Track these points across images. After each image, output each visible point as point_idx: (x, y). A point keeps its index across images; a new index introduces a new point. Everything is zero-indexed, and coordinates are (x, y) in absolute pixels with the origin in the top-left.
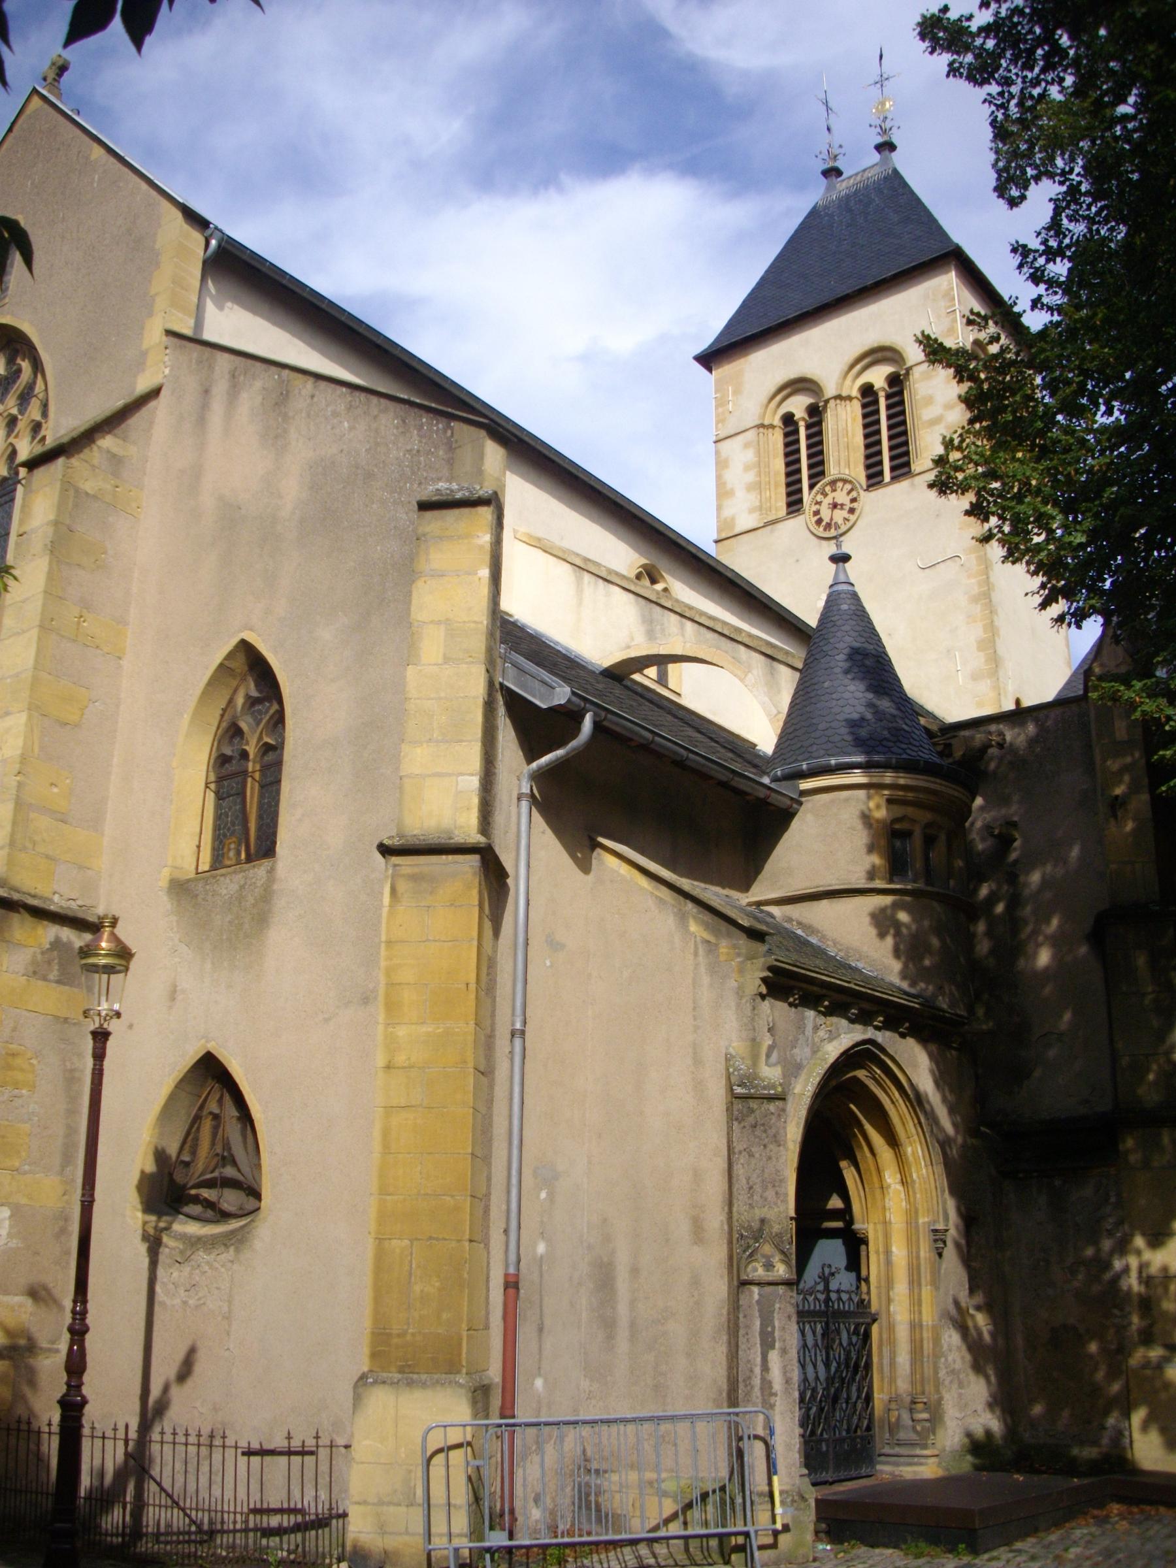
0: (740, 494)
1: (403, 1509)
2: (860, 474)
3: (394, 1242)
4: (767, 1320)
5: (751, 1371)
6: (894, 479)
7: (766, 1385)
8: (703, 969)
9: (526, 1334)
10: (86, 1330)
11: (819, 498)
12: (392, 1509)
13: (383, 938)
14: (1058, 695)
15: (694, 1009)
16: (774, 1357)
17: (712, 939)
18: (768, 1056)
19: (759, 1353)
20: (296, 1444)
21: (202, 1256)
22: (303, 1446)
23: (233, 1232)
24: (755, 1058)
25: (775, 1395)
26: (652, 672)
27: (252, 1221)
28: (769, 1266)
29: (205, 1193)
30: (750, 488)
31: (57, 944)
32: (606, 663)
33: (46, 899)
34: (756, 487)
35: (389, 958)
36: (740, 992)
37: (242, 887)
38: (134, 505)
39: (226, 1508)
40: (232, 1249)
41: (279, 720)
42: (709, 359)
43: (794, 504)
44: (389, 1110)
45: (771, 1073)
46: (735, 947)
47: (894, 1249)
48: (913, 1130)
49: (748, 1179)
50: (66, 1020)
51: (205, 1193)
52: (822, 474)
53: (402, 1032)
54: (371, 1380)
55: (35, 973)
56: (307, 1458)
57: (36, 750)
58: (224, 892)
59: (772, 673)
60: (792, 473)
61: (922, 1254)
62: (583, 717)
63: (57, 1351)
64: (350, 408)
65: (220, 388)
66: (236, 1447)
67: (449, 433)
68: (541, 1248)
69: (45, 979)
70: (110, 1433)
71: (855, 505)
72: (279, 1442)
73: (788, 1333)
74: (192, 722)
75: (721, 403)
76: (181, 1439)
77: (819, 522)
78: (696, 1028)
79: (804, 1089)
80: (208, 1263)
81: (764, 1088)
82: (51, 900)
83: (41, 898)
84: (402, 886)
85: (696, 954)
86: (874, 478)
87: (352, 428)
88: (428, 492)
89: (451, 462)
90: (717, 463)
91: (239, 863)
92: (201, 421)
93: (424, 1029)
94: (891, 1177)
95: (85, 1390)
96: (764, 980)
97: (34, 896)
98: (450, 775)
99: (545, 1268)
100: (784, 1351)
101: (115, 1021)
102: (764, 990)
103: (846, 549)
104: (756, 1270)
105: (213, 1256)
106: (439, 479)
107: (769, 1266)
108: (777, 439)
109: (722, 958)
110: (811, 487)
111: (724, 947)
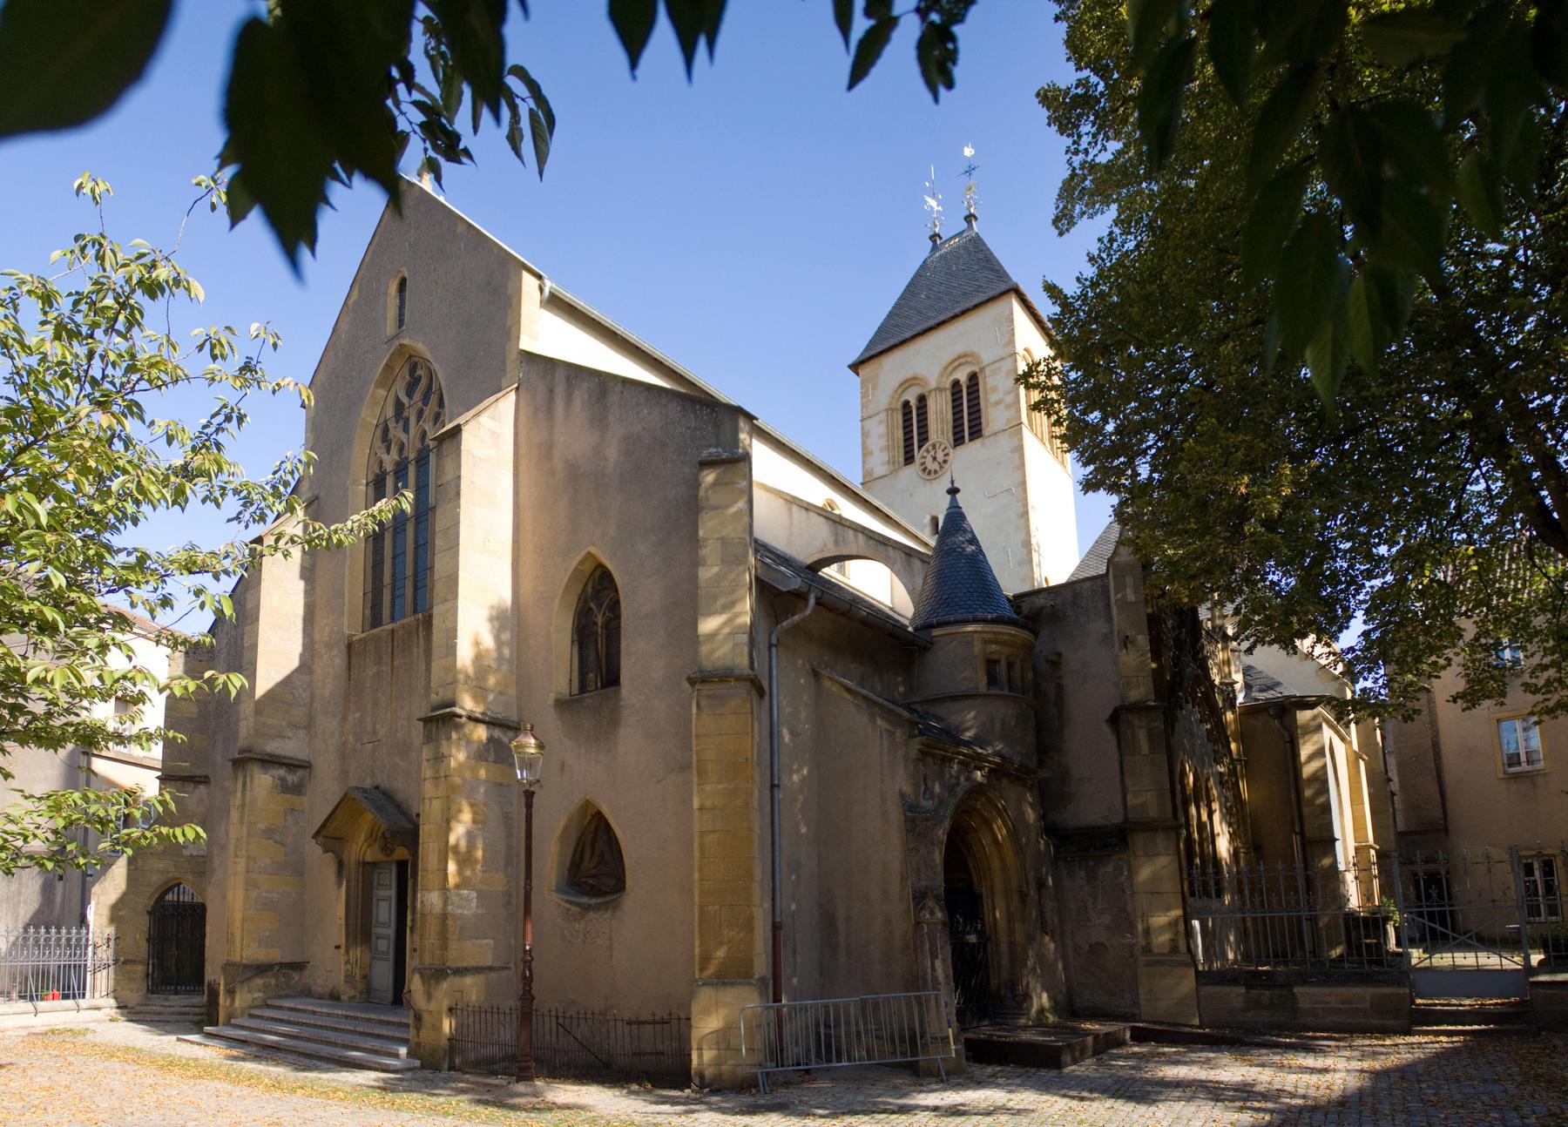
0: (877, 453)
6: (970, 440)
7: (935, 978)
14: (1073, 575)
16: (938, 963)
20: (658, 1018)
21: (591, 915)
26: (835, 566)
28: (932, 913)
30: (882, 450)
32: (809, 561)
34: (887, 448)
35: (698, 745)
41: (615, 605)
42: (855, 367)
50: (501, 784)
52: (926, 439)
53: (708, 788)
59: (909, 564)
65: (560, 390)
69: (486, 760)
72: (645, 1016)
75: (864, 395)
76: (589, 1015)
78: (882, 781)
84: (704, 703)
85: (881, 738)
86: (958, 441)
90: (863, 434)
91: (596, 689)
93: (720, 786)
100: (944, 960)
106: (710, 446)
107: (932, 913)
108: (899, 417)
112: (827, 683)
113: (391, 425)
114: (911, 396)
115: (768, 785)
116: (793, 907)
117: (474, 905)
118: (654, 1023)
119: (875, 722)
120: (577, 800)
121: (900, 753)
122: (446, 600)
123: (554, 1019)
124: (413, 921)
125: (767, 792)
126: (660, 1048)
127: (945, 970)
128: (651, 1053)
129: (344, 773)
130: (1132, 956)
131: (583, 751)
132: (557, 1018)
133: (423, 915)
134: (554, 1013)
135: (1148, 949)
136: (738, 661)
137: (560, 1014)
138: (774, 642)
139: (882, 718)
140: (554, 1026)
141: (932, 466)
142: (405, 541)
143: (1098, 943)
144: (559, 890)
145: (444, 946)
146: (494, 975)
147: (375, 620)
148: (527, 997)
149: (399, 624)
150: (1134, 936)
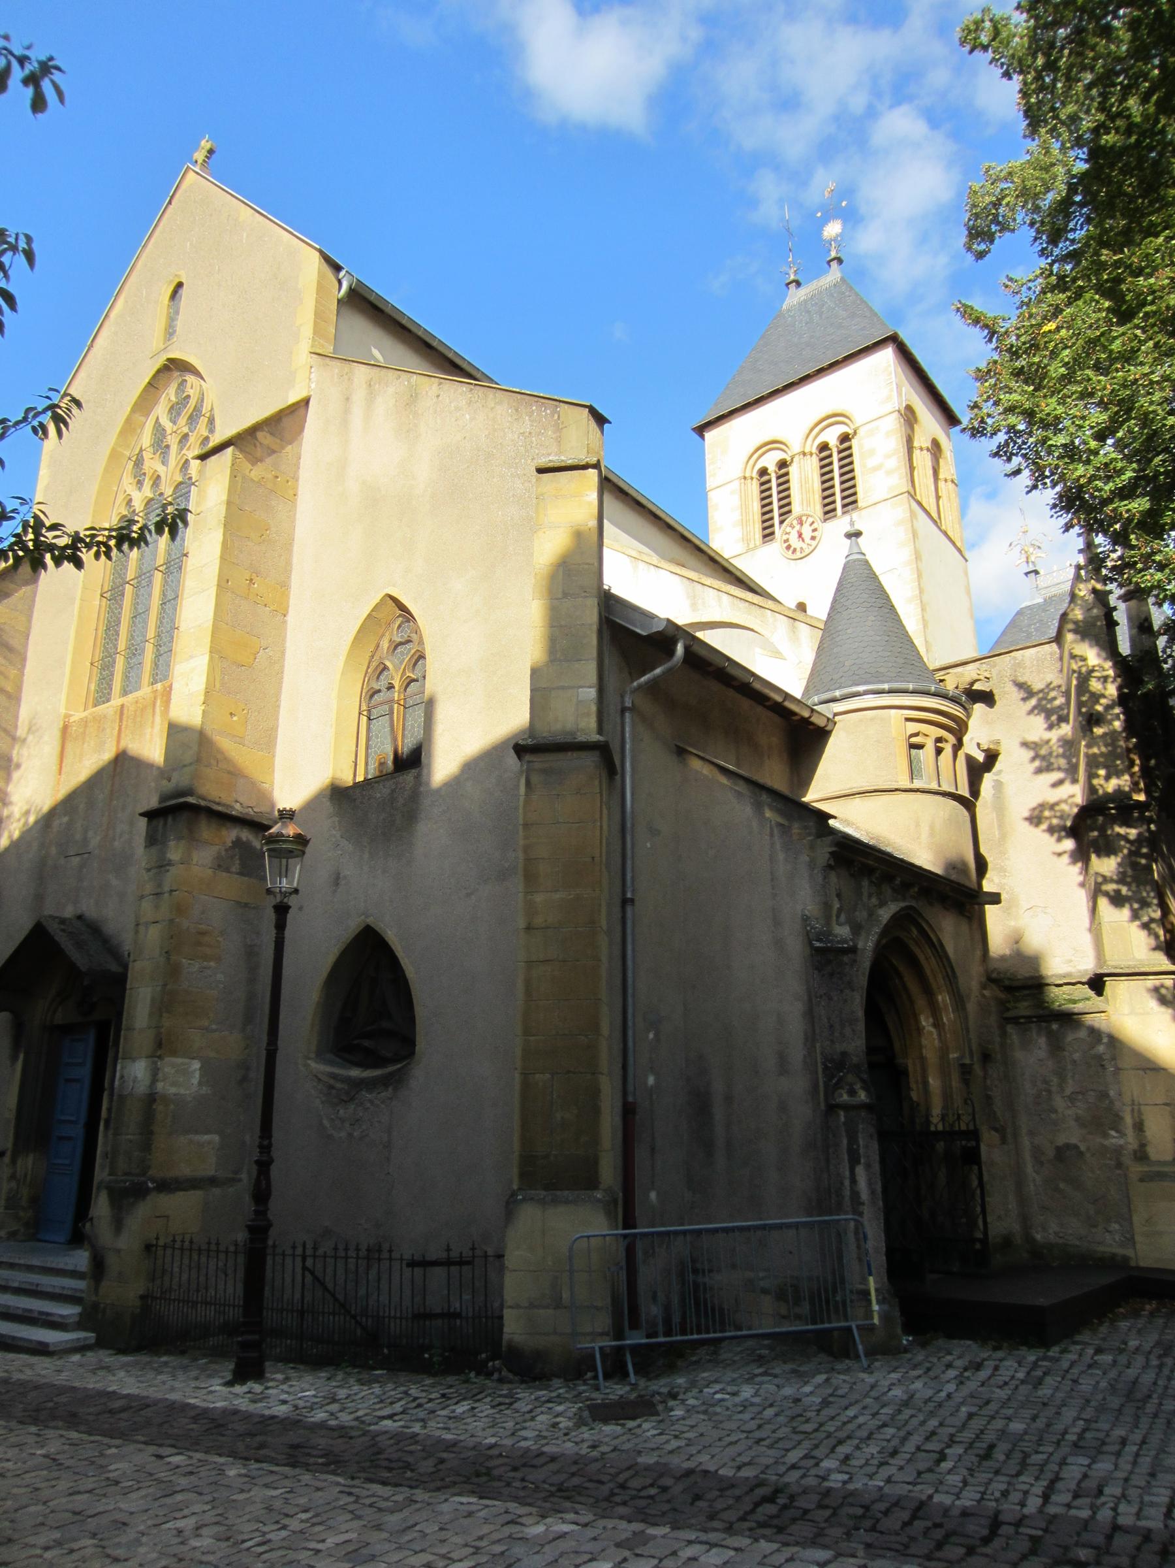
1: (550, 1311)
2: (818, 510)
3: (537, 1076)
4: (852, 1137)
5: (842, 1184)
6: (844, 513)
7: (855, 1195)
8: (778, 846)
9: (641, 1154)
10: (270, 1162)
11: (789, 529)
12: (542, 1311)
13: (521, 822)
15: (772, 880)
16: (860, 1170)
17: (786, 823)
18: (838, 917)
19: (847, 1168)
20: (454, 1254)
22: (461, 1257)
23: (391, 1074)
24: (828, 918)
25: (863, 1204)
27: (409, 1063)
28: (852, 1093)
29: (366, 1043)
31: (238, 843)
33: (228, 806)
35: (526, 838)
36: (812, 865)
37: (393, 791)
38: (291, 492)
39: (392, 1314)
40: (390, 1089)
43: (768, 535)
44: (530, 964)
45: (842, 931)
46: (806, 828)
47: (931, 1080)
48: (942, 982)
49: (829, 1019)
50: (246, 905)
51: (366, 1043)
53: (539, 898)
54: (520, 1197)
55: (219, 866)
56: (465, 1268)
57: (218, 685)
58: (378, 795)
59: (794, 630)
60: (766, 512)
61: (954, 1084)
62: (675, 644)
63: (240, 1180)
64: (470, 403)
65: (359, 396)
66: (402, 1259)
67: (556, 417)
68: (651, 1080)
69: (228, 870)
70: (289, 1251)
71: (815, 534)
72: (435, 1253)
73: (869, 1147)
74: (346, 662)
77: (788, 547)
79: (868, 944)
80: (371, 1101)
81: (838, 942)
82: (232, 807)
83: (224, 805)
84: (535, 779)
85: (772, 835)
86: (829, 512)
87: (472, 419)
88: (544, 462)
89: (559, 440)
92: (345, 423)
93: (557, 896)
94: (926, 1022)
95: (270, 1216)
96: (832, 854)
97: (218, 804)
98: (573, 687)
99: (654, 1097)
100: (868, 1166)
101: (294, 896)
102: (832, 862)
103: (858, 527)
104: (841, 1096)
105: (374, 1095)
107: (852, 1093)
108: (754, 488)
109: (795, 837)
110: (782, 522)
111: (796, 829)
112: (696, 764)
113: (147, 455)
114: (770, 461)
115: (617, 901)
116: (651, 1080)
117: (195, 1081)
118: (448, 1263)
119: (761, 814)
120: (353, 926)
121: (804, 858)
122: (191, 657)
123: (299, 1260)
124: (109, 1110)
125: (617, 910)
126: (456, 1305)
127: (870, 1184)
128: (442, 1315)
129: (39, 898)
130: (1119, 1165)
131: (366, 856)
132: (304, 1258)
133: (122, 1098)
134: (299, 1251)
135: (1141, 1155)
136: (582, 724)
137: (309, 1252)
138: (628, 704)
139: (771, 808)
140: (299, 1270)
141: (795, 542)
142: (150, 595)
143: (1068, 1146)
144: (320, 1056)
145: (146, 1145)
146: (216, 1191)
147: (103, 695)
148: (259, 1230)
149: (131, 697)
150: (1122, 1134)
